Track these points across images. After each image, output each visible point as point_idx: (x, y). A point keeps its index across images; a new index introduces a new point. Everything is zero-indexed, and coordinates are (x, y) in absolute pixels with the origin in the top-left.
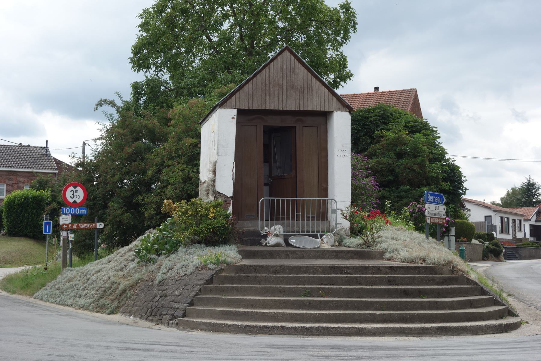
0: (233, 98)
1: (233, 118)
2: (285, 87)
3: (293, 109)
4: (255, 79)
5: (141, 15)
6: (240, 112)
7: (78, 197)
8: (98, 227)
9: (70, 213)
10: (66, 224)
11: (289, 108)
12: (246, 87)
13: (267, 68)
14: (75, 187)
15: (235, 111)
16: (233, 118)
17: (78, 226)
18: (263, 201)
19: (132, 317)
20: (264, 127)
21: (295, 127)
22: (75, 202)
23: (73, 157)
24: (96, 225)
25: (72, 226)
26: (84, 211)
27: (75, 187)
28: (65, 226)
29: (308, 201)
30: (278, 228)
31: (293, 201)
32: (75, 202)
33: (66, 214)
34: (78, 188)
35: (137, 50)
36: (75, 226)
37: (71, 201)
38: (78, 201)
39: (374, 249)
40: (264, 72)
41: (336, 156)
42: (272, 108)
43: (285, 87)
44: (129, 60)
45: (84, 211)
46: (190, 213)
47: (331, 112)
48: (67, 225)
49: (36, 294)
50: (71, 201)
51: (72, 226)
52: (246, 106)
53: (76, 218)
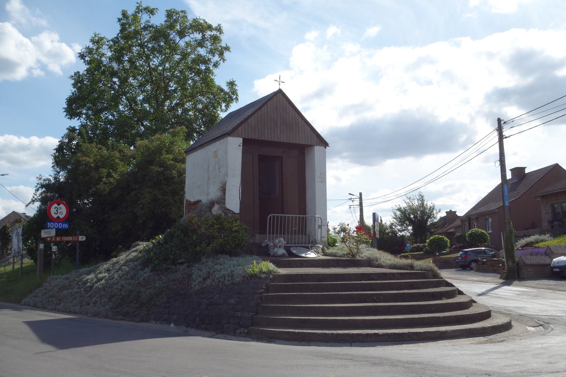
0: (240, 128)
1: (239, 146)
2: (279, 123)
3: (285, 141)
4: (256, 114)
5: (72, 77)
6: (246, 142)
7: (61, 213)
8: (80, 240)
9: (54, 227)
10: (50, 237)
11: (282, 140)
12: (249, 120)
13: (265, 106)
14: (59, 205)
15: (240, 140)
16: (239, 146)
17: (61, 239)
18: (271, 217)
19: (172, 325)
20: (259, 155)
21: (282, 157)
22: (58, 217)
23: (40, 179)
24: (78, 238)
25: (56, 239)
26: (66, 226)
27: (59, 205)
28: (48, 239)
29: (292, 217)
30: (282, 241)
31: (281, 217)
32: (58, 217)
33: (50, 228)
34: (62, 206)
35: (71, 101)
36: (58, 239)
37: (55, 216)
38: (62, 216)
39: (358, 258)
40: (263, 109)
41: (316, 182)
42: (270, 140)
43: (279, 123)
44: (64, 110)
45: (66, 226)
46: (216, 227)
47: (311, 146)
48: (51, 238)
49: (23, 301)
50: (55, 216)
51: (56, 239)
52: (250, 136)
53: (59, 232)
